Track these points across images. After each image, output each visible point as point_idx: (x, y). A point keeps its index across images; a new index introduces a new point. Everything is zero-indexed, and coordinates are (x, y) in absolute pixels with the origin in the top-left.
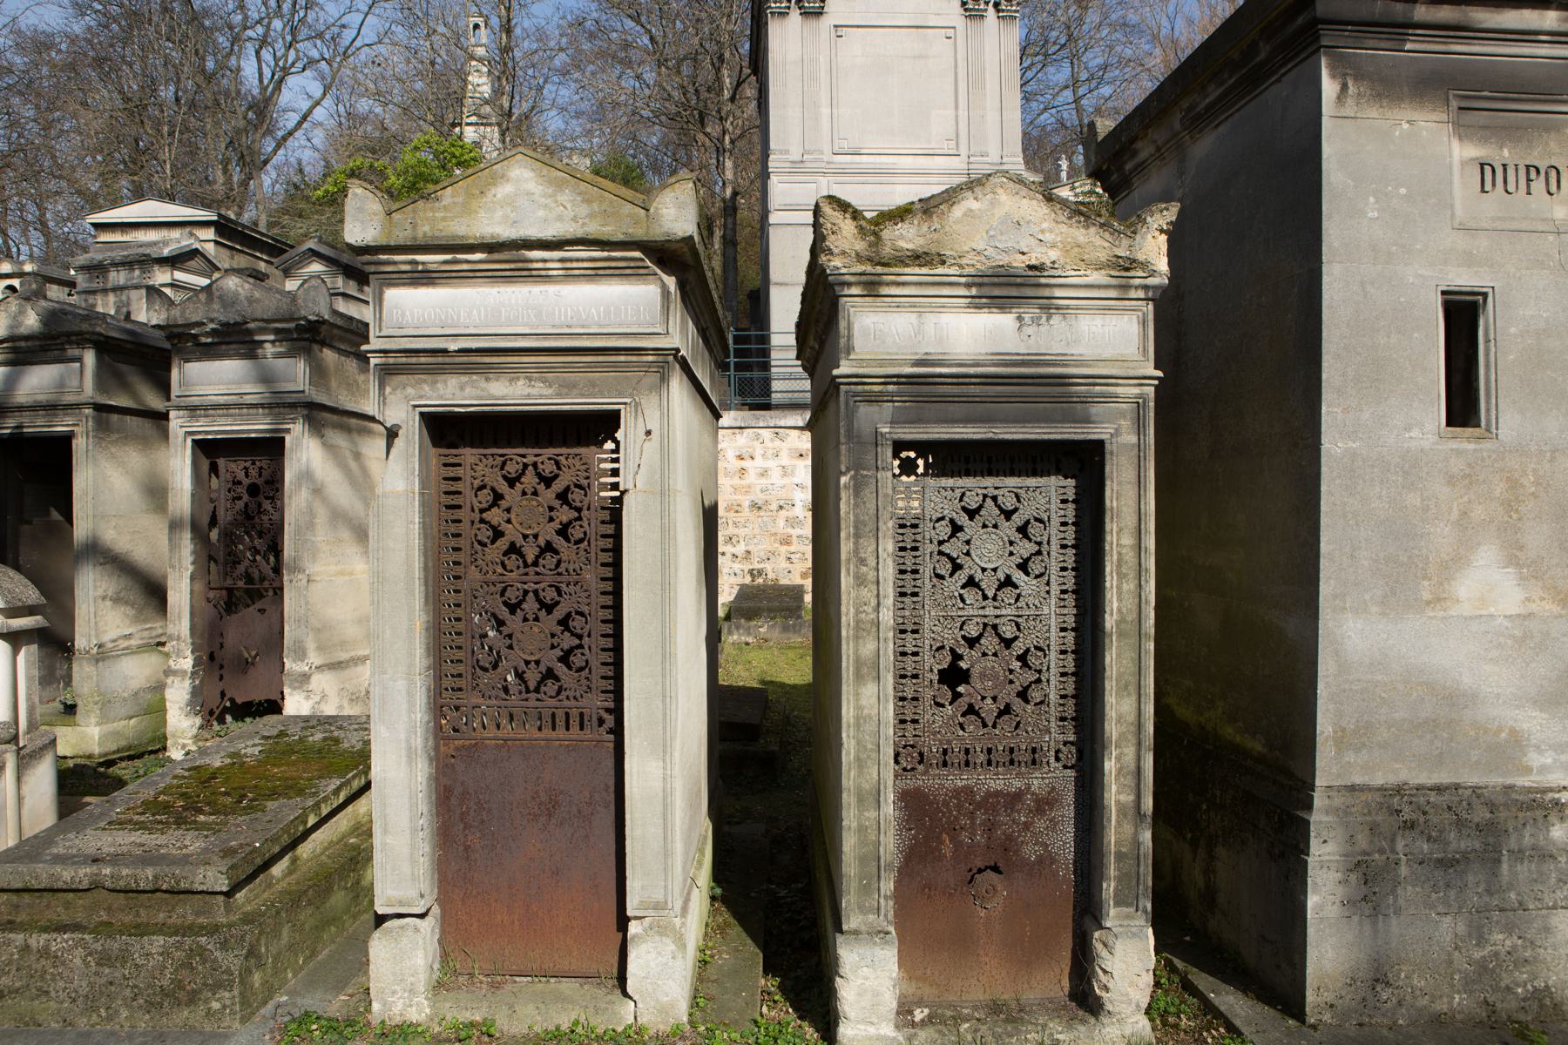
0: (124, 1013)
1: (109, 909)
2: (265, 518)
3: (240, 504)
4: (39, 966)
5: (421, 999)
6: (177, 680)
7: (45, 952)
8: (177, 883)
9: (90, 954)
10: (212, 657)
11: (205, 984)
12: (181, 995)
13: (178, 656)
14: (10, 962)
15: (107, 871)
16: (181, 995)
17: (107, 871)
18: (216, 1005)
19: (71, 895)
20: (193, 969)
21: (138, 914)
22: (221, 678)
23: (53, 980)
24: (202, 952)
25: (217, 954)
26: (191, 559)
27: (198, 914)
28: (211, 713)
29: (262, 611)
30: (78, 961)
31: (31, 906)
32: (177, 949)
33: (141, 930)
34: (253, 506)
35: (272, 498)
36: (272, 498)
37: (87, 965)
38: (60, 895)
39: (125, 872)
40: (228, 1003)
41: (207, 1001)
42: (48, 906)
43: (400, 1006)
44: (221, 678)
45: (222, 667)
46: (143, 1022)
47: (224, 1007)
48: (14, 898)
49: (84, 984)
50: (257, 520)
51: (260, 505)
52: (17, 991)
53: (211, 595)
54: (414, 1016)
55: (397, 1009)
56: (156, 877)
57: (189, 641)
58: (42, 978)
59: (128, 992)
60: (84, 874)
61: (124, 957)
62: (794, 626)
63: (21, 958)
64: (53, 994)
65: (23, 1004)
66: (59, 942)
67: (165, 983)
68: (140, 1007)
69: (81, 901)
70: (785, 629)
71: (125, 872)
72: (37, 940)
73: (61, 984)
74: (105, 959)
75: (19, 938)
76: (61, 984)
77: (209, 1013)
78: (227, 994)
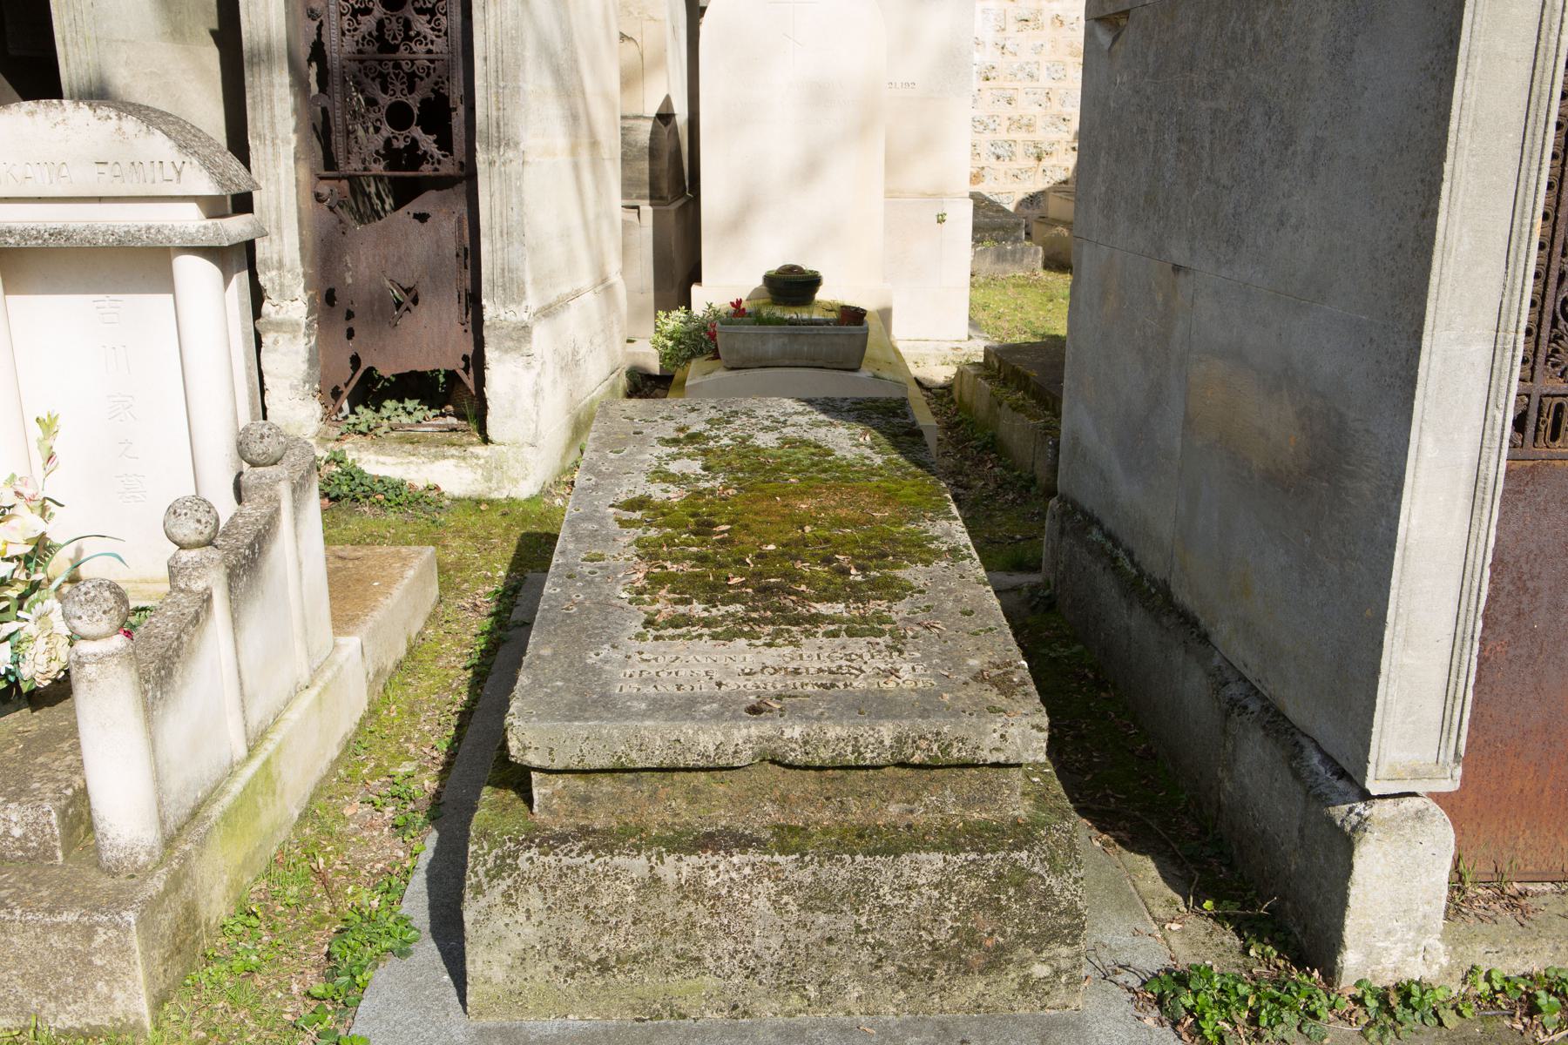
0: (855, 990)
1: (783, 801)
2: (420, 49)
3: (368, 24)
4: (681, 915)
5: (1433, 941)
6: (283, 338)
7: (692, 889)
8: (945, 750)
9: (788, 890)
10: (330, 298)
11: (1023, 936)
12: (973, 956)
13: (282, 296)
14: (619, 909)
15: (795, 731)
16: (973, 956)
17: (795, 731)
18: (1040, 970)
19: (703, 776)
20: (999, 909)
21: (843, 808)
22: (350, 334)
23: (711, 937)
24: (1020, 880)
25: (1051, 881)
26: (291, 122)
27: (968, 803)
28: (336, 393)
29: (422, 217)
30: (762, 904)
31: (616, 799)
32: (970, 875)
33: (894, 843)
34: (394, 26)
35: (432, 12)
36: (432, 12)
37: (781, 909)
38: (677, 776)
39: (833, 732)
40: (1065, 964)
41: (1022, 964)
42: (653, 797)
43: (1396, 954)
44: (350, 334)
45: (350, 315)
46: (892, 1006)
47: (1057, 973)
48: (580, 784)
49: (775, 943)
50: (403, 53)
51: (407, 25)
52: (635, 959)
53: (324, 188)
54: (1415, 970)
55: (1388, 962)
56: (900, 740)
57: (300, 270)
58: (687, 935)
59: (865, 956)
60: (745, 736)
61: (859, 892)
62: (1013, 253)
63: (644, 900)
64: (710, 962)
65: (650, 982)
66: (720, 870)
67: (942, 935)
68: (888, 979)
69: (720, 788)
70: (1001, 257)
71: (833, 732)
72: (676, 869)
73: (729, 944)
74: (819, 899)
75: (638, 865)
76: (729, 944)
77: (1026, 985)
78: (1065, 951)
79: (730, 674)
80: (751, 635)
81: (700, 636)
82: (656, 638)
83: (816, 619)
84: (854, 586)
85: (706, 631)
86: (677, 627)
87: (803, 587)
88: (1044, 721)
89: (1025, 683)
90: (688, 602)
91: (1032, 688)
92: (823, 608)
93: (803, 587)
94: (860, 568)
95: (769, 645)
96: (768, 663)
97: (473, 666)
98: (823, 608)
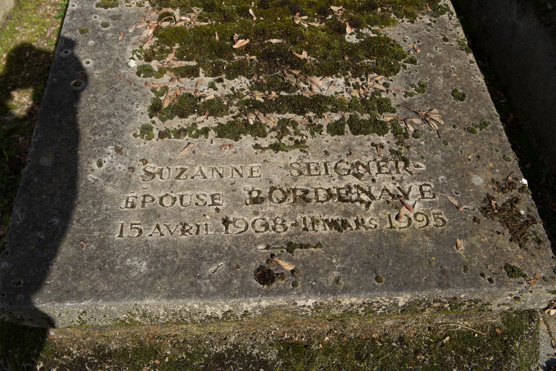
79: (236, 202)
80: (258, 130)
81: (206, 131)
82: (162, 135)
83: (319, 104)
84: (351, 50)
85: (211, 122)
86: (183, 115)
87: (304, 55)
88: (79, 152)
89: (534, 221)
90: (192, 72)
91: (539, 228)
92: (322, 85)
93: (304, 55)
94: (356, 25)
95: (276, 147)
96: (277, 181)
97: (141, 343)
98: (322, 85)
